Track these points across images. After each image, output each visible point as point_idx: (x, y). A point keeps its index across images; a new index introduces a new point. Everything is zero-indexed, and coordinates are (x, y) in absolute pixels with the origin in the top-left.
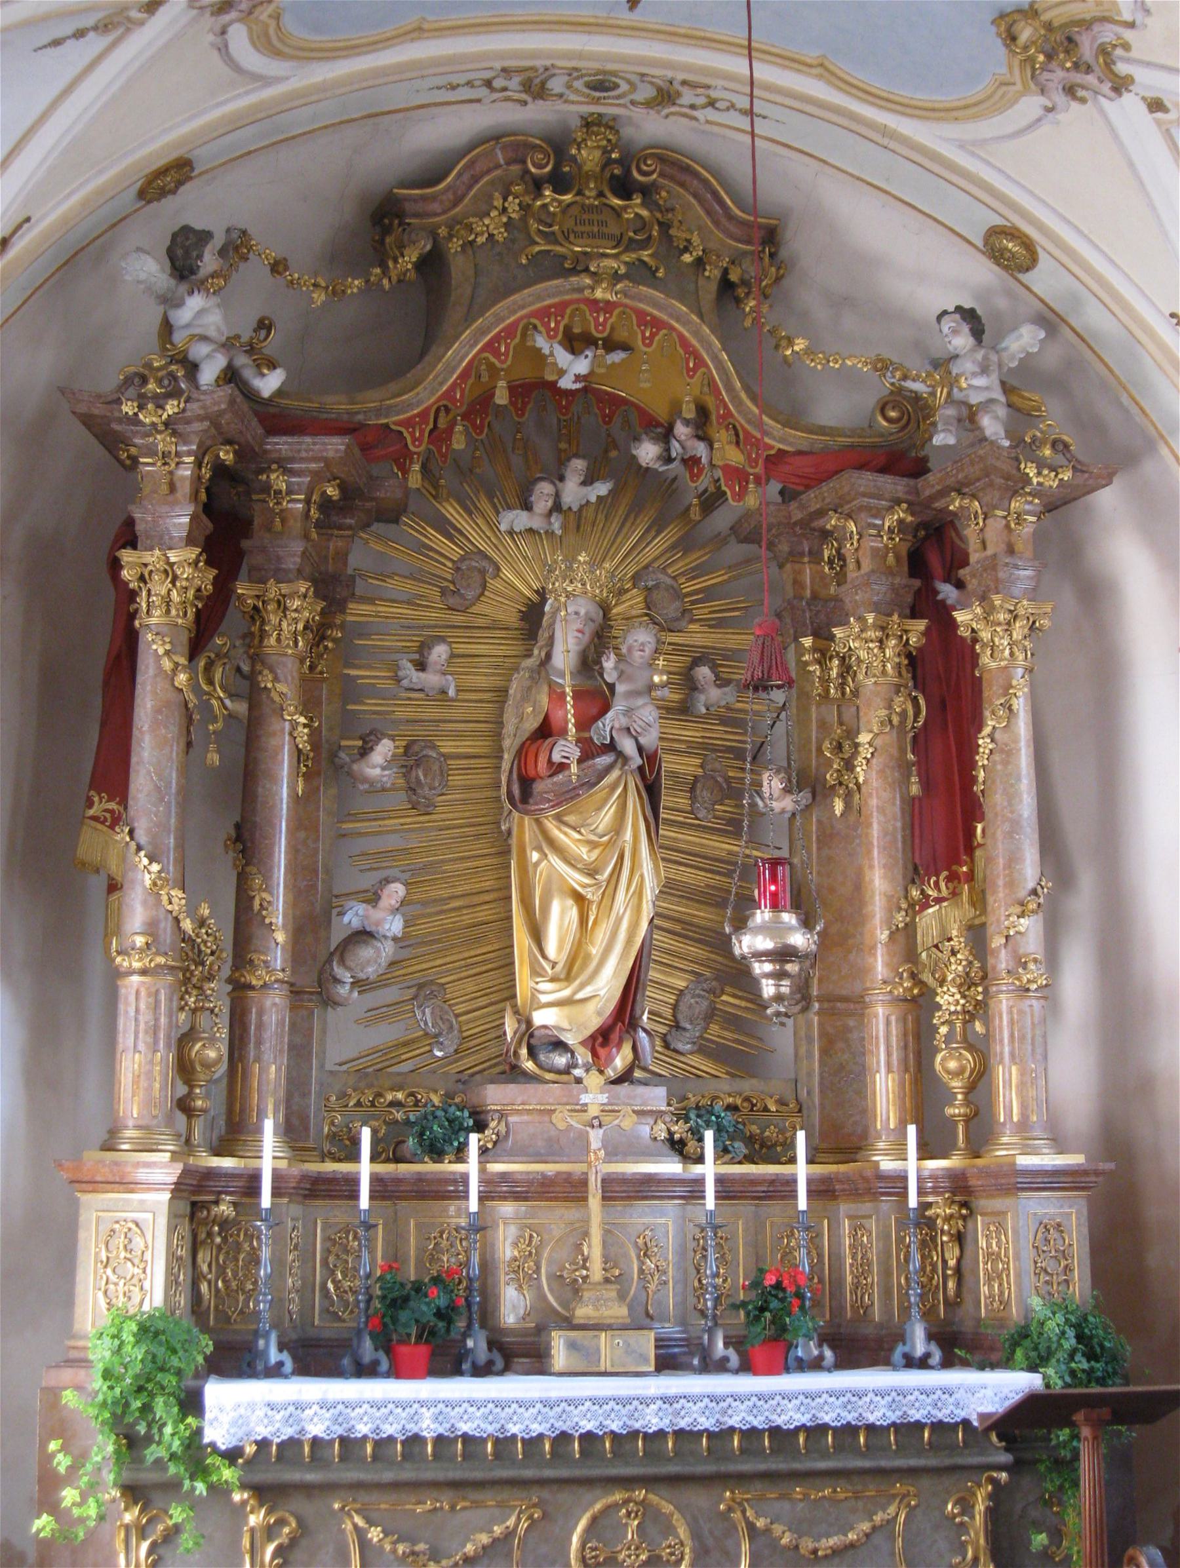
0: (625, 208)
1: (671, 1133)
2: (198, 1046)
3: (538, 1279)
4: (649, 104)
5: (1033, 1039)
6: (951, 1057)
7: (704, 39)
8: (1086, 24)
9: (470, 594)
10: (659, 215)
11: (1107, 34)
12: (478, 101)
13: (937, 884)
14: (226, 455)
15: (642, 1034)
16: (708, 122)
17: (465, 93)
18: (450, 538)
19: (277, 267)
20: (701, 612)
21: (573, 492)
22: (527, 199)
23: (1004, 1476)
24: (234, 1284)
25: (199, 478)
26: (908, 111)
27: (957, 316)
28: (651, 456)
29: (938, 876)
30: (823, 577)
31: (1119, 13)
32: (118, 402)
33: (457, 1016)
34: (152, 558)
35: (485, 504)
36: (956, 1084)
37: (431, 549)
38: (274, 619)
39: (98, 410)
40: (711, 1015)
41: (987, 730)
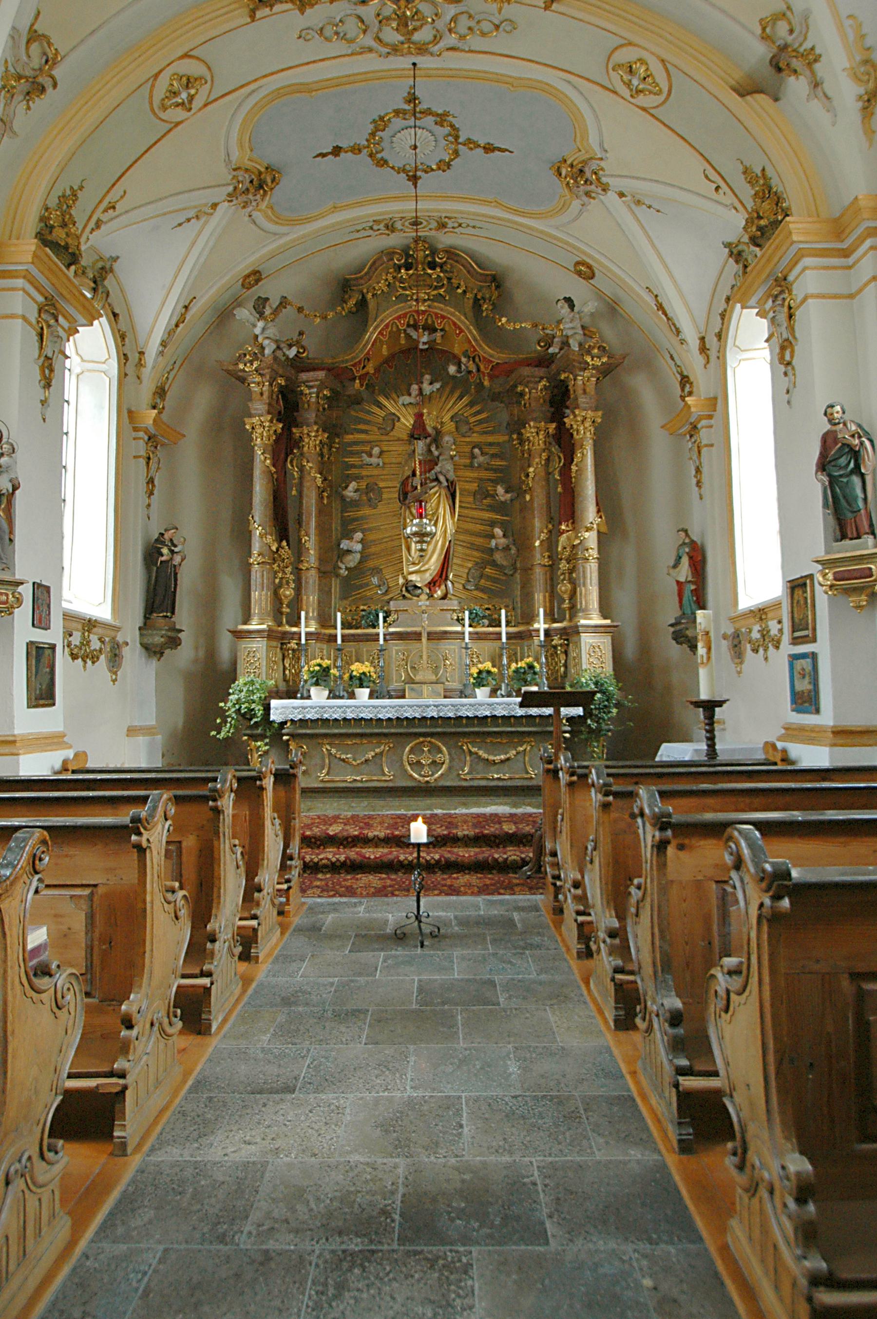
4: (437, 229)
8: (585, 162)
11: (594, 165)
14: (281, 381)
17: (363, 234)
19: (300, 310)
20: (477, 429)
22: (395, 274)
23: (567, 735)
30: (522, 411)
31: (596, 154)
32: (237, 364)
34: (255, 420)
35: (394, 396)
36: (566, 596)
38: (306, 440)
39: (231, 368)
40: (481, 577)
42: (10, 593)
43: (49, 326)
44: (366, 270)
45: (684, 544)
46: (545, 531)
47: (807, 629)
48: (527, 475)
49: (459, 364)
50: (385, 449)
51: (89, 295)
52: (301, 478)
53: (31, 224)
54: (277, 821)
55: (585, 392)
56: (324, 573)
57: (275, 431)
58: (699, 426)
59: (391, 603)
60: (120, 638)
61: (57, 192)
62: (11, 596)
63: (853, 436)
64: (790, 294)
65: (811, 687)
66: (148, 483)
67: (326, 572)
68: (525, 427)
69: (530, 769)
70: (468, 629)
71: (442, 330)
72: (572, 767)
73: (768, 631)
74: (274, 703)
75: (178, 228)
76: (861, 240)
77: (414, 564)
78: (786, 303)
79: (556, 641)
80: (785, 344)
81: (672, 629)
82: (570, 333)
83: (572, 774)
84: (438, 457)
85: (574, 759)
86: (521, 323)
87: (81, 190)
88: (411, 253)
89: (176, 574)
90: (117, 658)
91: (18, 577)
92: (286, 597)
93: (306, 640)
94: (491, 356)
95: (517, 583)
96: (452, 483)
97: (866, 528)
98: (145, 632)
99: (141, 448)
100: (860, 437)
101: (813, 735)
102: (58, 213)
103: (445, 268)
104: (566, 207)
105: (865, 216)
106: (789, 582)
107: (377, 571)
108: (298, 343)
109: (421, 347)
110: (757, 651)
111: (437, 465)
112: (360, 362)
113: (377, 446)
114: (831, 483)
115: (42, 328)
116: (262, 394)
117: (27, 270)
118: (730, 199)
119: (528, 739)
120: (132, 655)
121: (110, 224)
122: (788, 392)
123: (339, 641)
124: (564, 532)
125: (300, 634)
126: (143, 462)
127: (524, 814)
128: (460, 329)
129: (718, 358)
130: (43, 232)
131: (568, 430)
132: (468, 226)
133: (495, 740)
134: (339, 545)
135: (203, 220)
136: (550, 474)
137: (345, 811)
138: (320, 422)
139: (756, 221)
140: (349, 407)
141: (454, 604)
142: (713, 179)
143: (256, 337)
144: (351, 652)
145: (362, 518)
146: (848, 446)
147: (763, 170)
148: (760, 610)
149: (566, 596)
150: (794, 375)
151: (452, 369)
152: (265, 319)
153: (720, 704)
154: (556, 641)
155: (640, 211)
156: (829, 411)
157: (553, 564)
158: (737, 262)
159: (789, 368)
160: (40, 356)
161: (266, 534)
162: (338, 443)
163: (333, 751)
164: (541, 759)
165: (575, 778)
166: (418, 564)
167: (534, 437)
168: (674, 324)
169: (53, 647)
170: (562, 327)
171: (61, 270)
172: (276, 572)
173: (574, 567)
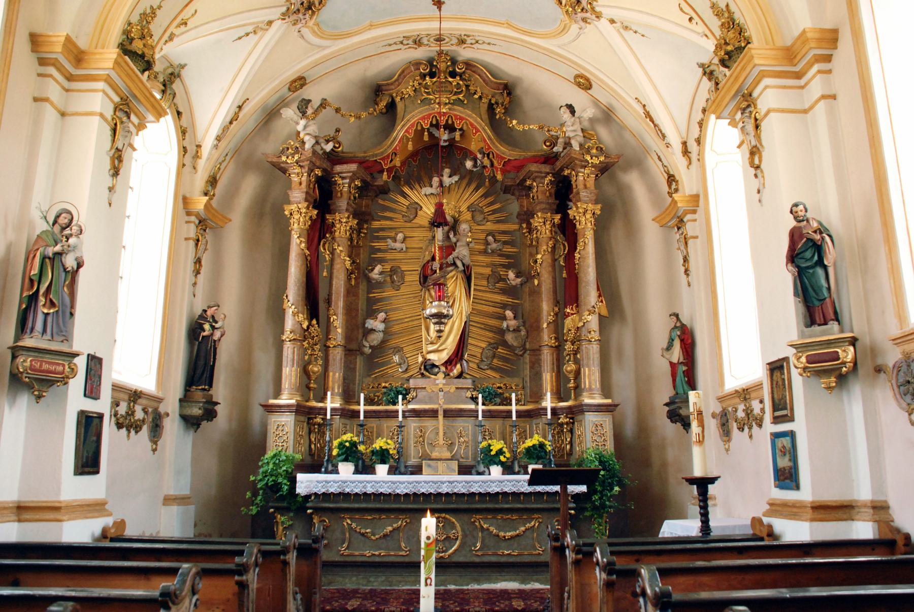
0: (453, 81)
1: (472, 395)
2: (311, 366)
3: (424, 444)
5: (593, 359)
6: (569, 366)
7: (467, 19)
9: (412, 217)
10: (465, 83)
12: (400, 49)
13: (572, 308)
14: (318, 172)
15: (464, 362)
16: (478, 49)
18: (405, 198)
19: (337, 110)
20: (491, 218)
21: (447, 181)
22: (421, 81)
23: (573, 512)
24: (322, 445)
25: (310, 180)
26: (541, 36)
27: (565, 107)
28: (469, 166)
29: (573, 306)
32: (280, 157)
33: (407, 358)
34: (294, 207)
35: (417, 186)
37: (399, 202)
38: (338, 226)
39: (275, 160)
40: (494, 356)
41: (578, 250)
42: (66, 364)
43: (122, 122)
44: (396, 77)
45: (675, 327)
46: (552, 314)
47: (786, 409)
48: (536, 262)
49: (475, 160)
50: (408, 234)
51: (158, 96)
52: (332, 260)
53: (115, 36)
54: (299, 596)
55: (585, 187)
56: (349, 350)
57: (311, 217)
58: (685, 220)
59: (411, 381)
60: (162, 409)
61: (140, 10)
62: (67, 367)
63: (815, 232)
64: (755, 108)
65: (790, 464)
66: (195, 263)
67: (351, 350)
68: (534, 217)
69: (537, 545)
70: (481, 408)
71: (460, 130)
72: (577, 545)
73: (752, 411)
74: (300, 477)
75: (238, 41)
76: (810, 65)
77: (432, 343)
78: (753, 116)
79: (563, 419)
80: (754, 150)
81: (667, 409)
82: (571, 135)
83: (577, 553)
84: (456, 244)
85: (579, 536)
86: (529, 125)
87: (159, 9)
88: (435, 64)
89: (215, 349)
90: (158, 429)
91: (76, 348)
92: (314, 373)
93: (331, 415)
94: (503, 154)
95: (526, 363)
96: (468, 267)
97: (832, 316)
98: (185, 404)
99: (192, 231)
100: (821, 233)
101: (795, 510)
102: (139, 27)
103: (464, 77)
104: (564, 32)
105: (813, 45)
106: (768, 364)
107: (398, 350)
108: (334, 139)
109: (442, 144)
110: (743, 430)
111: (454, 251)
112: (388, 156)
113: (401, 232)
114: (799, 273)
115: (116, 124)
116: (301, 184)
117: (108, 75)
118: (701, 28)
119: (536, 516)
120: (172, 426)
121: (180, 37)
122: (759, 192)
123: (362, 417)
124: (568, 315)
125: (326, 409)
126: (192, 243)
127: (532, 590)
128: (476, 128)
129: (699, 160)
130: (124, 43)
131: (571, 220)
132: (484, 43)
133: (505, 517)
134: (364, 323)
135: (260, 33)
136: (556, 260)
137: (363, 585)
138: (351, 209)
139: (724, 47)
140: (376, 196)
141: (468, 383)
142: (686, 11)
143: (299, 133)
144: (373, 427)
145: (389, 298)
146: (812, 240)
147: (727, 6)
148: (744, 390)
149: (571, 376)
150: (763, 177)
151: (469, 164)
152: (307, 118)
153: (712, 480)
154: (563, 419)
155: (628, 35)
156: (794, 209)
157: (559, 346)
158: (710, 80)
159: (759, 171)
160: (111, 148)
161: (298, 313)
162: (367, 229)
163: (354, 525)
164: (549, 536)
165: (580, 556)
166: (436, 344)
167: (541, 226)
168: (660, 130)
169: (101, 417)
170: (564, 129)
171: (137, 76)
172: (306, 349)
173: (578, 348)
